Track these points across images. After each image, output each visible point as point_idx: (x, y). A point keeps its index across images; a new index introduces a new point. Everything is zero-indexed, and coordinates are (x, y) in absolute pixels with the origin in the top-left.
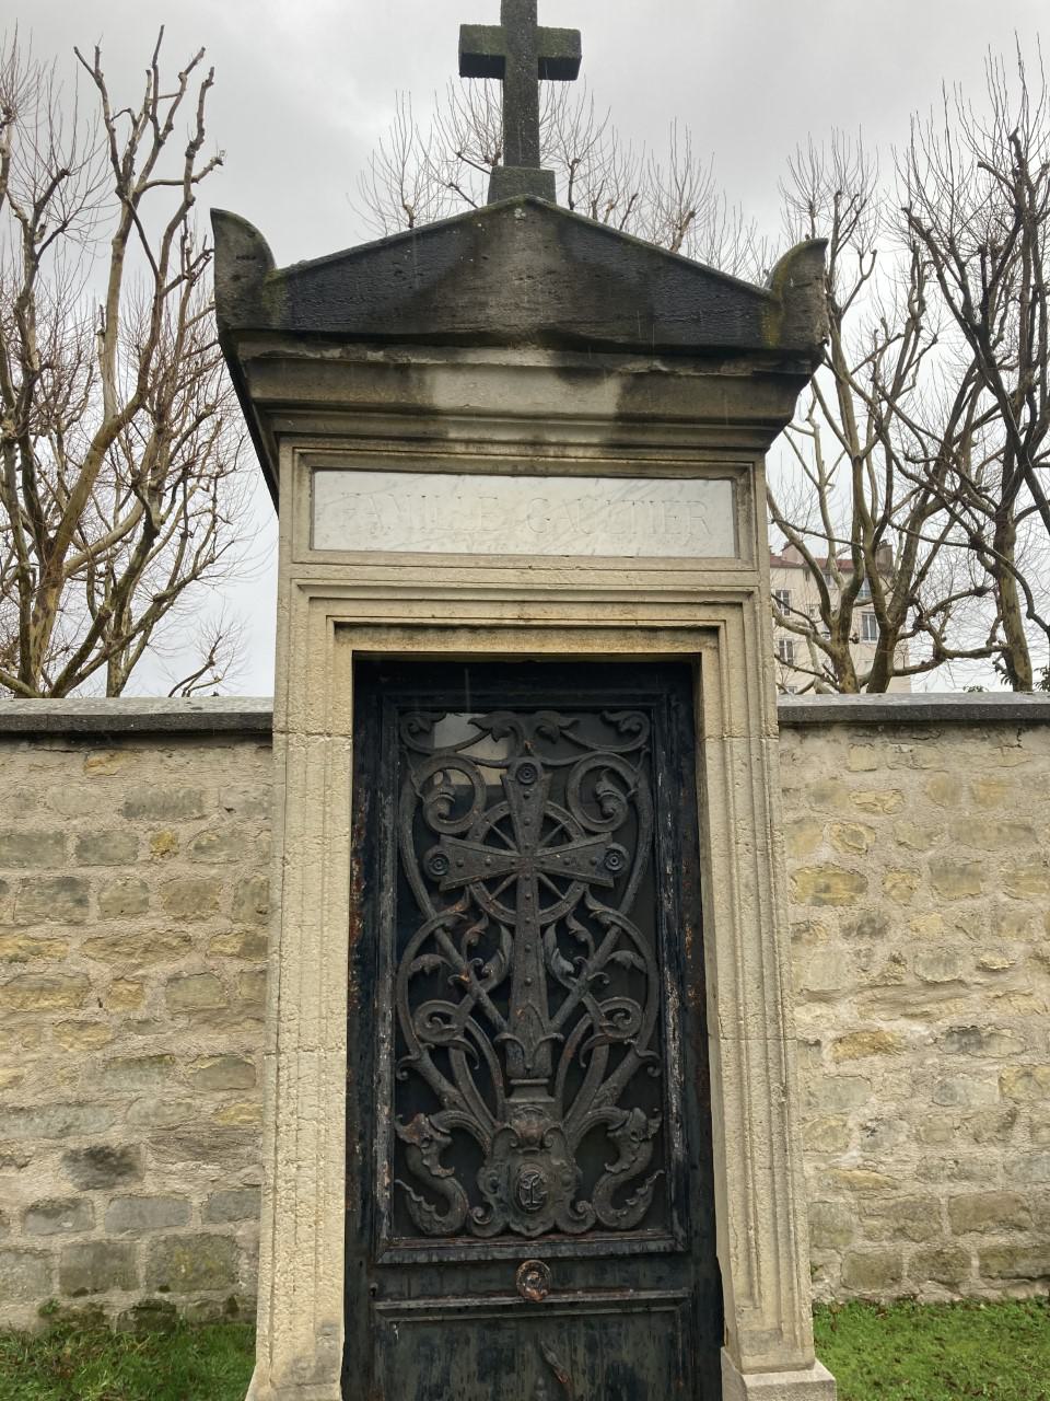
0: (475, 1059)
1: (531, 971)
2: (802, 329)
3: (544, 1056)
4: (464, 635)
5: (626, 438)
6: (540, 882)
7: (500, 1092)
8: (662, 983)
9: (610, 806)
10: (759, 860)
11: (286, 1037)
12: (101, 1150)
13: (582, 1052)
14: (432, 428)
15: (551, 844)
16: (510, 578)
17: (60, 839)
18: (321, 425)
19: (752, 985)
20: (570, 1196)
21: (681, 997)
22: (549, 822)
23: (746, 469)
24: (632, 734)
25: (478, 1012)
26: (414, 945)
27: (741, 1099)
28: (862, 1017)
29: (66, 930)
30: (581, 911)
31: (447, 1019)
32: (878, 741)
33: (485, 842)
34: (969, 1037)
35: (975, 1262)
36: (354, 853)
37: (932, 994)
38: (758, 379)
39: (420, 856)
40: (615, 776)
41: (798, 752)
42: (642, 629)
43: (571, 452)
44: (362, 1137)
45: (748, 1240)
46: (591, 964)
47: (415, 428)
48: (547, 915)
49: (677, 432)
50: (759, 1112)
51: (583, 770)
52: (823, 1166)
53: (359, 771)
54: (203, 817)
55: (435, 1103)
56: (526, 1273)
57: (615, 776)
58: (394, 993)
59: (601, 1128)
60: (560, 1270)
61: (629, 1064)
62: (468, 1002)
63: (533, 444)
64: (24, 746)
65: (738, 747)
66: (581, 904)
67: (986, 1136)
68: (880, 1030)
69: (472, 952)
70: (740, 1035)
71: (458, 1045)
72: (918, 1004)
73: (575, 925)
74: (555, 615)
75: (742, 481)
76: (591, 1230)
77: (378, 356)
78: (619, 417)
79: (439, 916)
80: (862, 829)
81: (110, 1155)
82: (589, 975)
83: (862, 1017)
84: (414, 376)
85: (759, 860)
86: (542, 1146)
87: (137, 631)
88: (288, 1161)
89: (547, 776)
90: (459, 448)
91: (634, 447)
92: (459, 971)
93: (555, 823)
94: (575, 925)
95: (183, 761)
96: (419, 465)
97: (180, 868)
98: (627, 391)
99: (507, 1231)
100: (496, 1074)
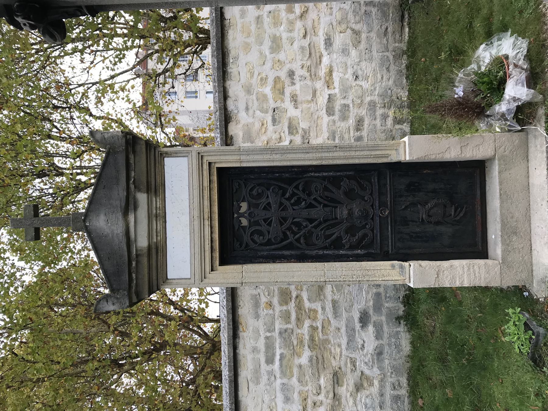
0: (328, 228)
1: (305, 213)
2: (118, 139)
3: (327, 209)
4: (213, 235)
5: (153, 190)
6: (281, 211)
7: (336, 221)
8: (308, 177)
9: (260, 191)
10: (275, 152)
11: (322, 280)
12: (360, 319)
13: (325, 198)
14: (153, 246)
15: (271, 207)
16: (197, 223)
17: (267, 338)
18: (154, 278)
19: (308, 155)
20: (363, 202)
21: (311, 172)
22: (265, 208)
23: (161, 154)
24: (239, 184)
25: (316, 227)
26: (298, 245)
27: (338, 159)
28: (321, 79)
29: (295, 334)
30: (289, 199)
31: (317, 235)
32: (229, 70)
33: (270, 226)
34: (328, 42)
35: (397, 45)
36: (274, 262)
37: (313, 55)
38: (134, 152)
39: (274, 244)
40: (251, 190)
41: (234, 99)
42: (210, 184)
43: (158, 206)
44: (349, 258)
45: (374, 157)
46: (303, 197)
47: (154, 251)
48: (290, 209)
49: (151, 175)
50: (341, 154)
51: (250, 199)
52: (367, 94)
53: (251, 262)
54: (259, 294)
55: (339, 238)
56: (382, 214)
57: (251, 190)
58: (311, 250)
59: (346, 194)
60: (383, 205)
61: (330, 186)
62: (313, 230)
63: (157, 217)
64: (237, 351)
65: (243, 158)
66: (287, 199)
67: (358, 39)
68: (325, 73)
69: (300, 229)
70: (321, 159)
71: (324, 232)
72: (316, 59)
73: (293, 201)
74: (207, 210)
75: (164, 155)
76: (372, 196)
77: (134, 263)
78: (148, 193)
79: (291, 239)
80: (259, 78)
81: (361, 317)
82: (306, 197)
83: (321, 79)
84: (139, 252)
85: (275, 152)
86: (350, 210)
87: (185, 313)
88: (353, 278)
89: (252, 209)
90: (159, 238)
91: (156, 187)
92: (305, 233)
93: (265, 206)
94: (293, 201)
95: (241, 302)
96: (164, 249)
97: (275, 301)
98: (140, 191)
99: (372, 219)
100: (331, 222)
